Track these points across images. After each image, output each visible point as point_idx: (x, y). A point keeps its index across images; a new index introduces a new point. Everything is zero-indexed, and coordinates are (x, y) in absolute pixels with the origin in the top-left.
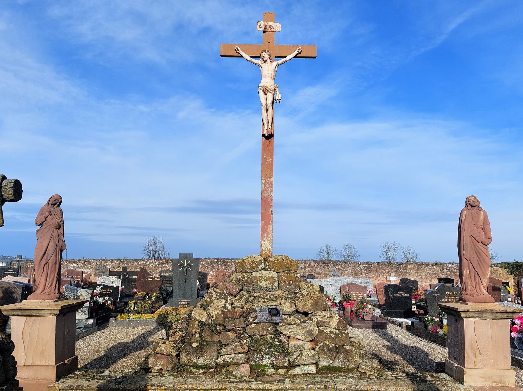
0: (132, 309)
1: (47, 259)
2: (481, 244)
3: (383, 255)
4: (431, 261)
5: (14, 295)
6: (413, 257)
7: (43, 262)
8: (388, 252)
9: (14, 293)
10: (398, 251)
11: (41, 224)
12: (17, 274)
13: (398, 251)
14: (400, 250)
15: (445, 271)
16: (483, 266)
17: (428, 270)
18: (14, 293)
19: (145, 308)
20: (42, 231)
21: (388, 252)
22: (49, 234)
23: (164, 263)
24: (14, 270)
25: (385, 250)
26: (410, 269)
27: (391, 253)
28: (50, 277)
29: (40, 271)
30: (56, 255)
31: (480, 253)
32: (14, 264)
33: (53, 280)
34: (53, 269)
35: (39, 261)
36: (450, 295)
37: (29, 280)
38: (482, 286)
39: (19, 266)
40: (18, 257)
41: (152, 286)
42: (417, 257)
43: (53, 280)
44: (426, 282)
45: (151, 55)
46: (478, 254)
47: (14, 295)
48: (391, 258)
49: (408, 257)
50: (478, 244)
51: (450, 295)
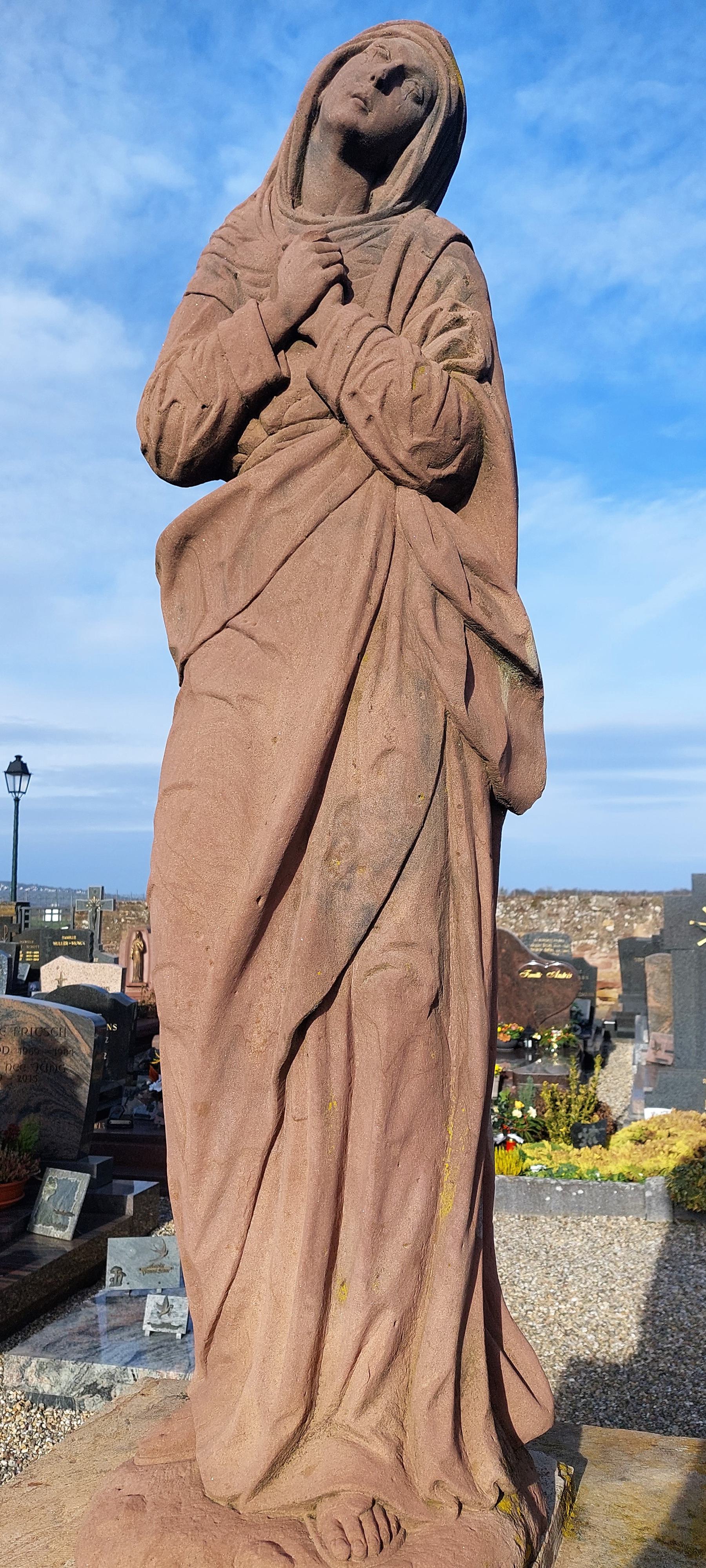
0: (517, 1113)
1: (321, 937)
5: (67, 1061)
7: (279, 990)
9: (64, 1051)
11: (214, 460)
12: (85, 952)
18: (64, 1051)
19: (569, 1110)
20: (230, 529)
22: (341, 559)
23: (522, 910)
24: (81, 935)
28: (379, 1228)
29: (228, 1116)
30: (443, 883)
32: (82, 915)
33: (420, 1260)
34: (412, 1089)
35: (209, 992)
37: (124, 971)
39: (95, 920)
40: (93, 891)
41: (541, 1000)
43: (420, 1260)
47: (67, 1061)
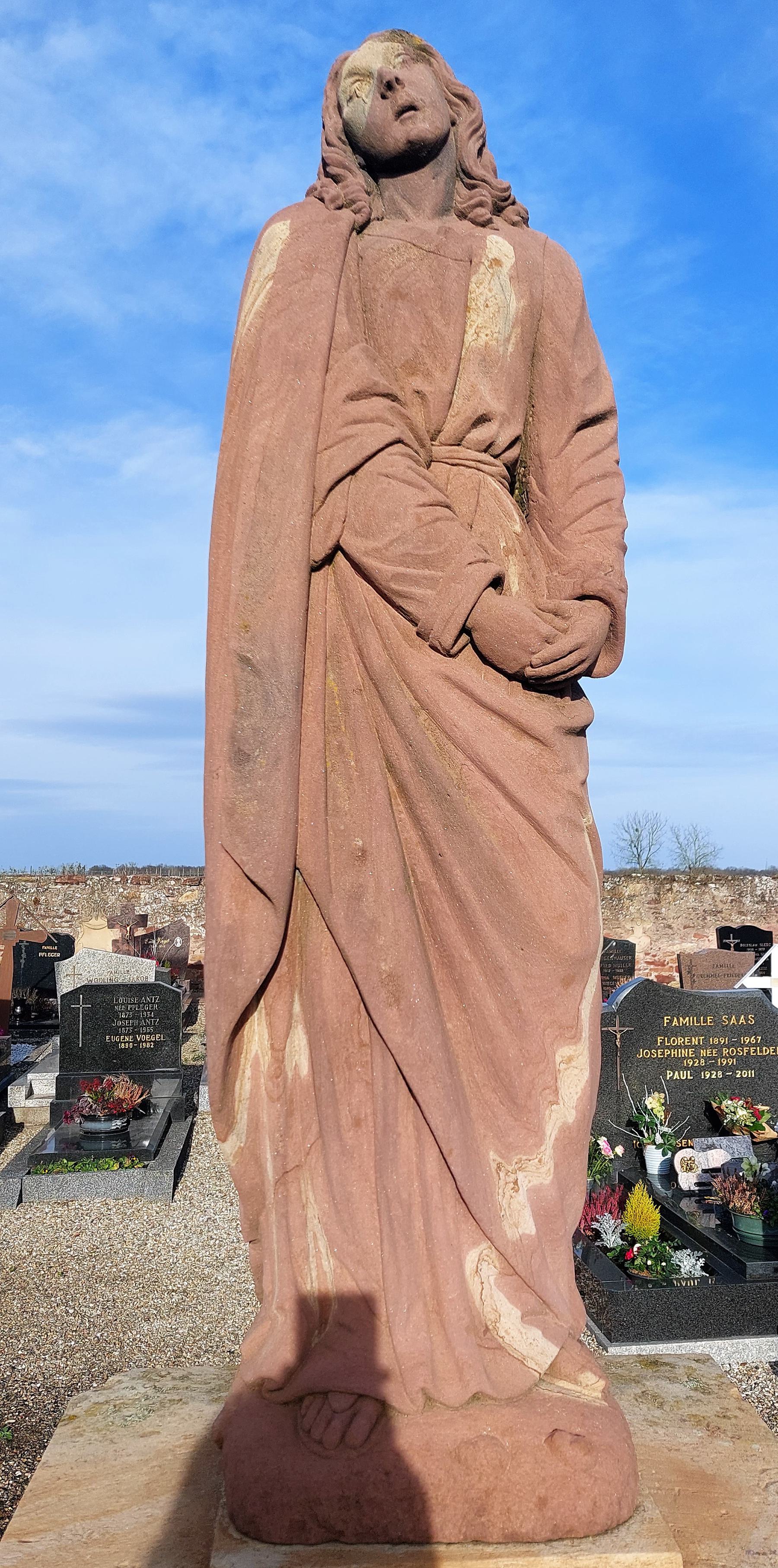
2: (467, 666)
3: (622, 849)
4: (759, 869)
6: (705, 855)
8: (635, 843)
10: (663, 839)
13: (663, 839)
14: (670, 834)
15: (747, 901)
16: (496, 974)
17: (691, 898)
21: (635, 843)
25: (626, 836)
26: (631, 897)
27: (644, 843)
31: (442, 797)
36: (683, 1031)
38: (481, 1270)
42: (715, 854)
44: (683, 939)
45: (81, 300)
46: (428, 811)
48: (644, 857)
49: (691, 855)
50: (424, 663)
51: (683, 1031)
